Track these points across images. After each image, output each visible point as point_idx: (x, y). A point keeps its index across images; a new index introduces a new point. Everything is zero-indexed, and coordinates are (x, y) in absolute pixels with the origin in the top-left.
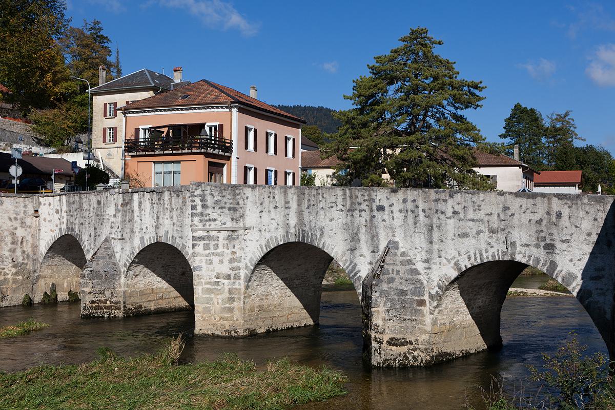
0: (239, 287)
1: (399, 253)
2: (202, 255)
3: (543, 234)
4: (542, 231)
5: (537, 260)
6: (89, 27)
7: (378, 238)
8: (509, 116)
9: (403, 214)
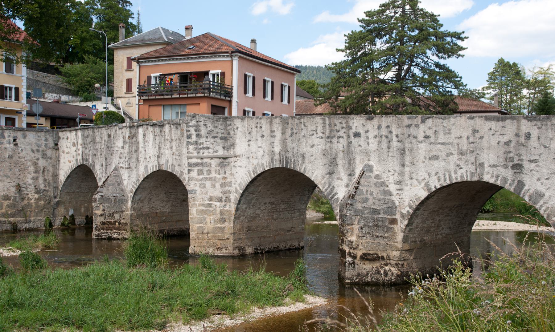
1: (373, 175)
2: (197, 180)
3: (511, 155)
4: (510, 152)
5: (505, 180)
7: (354, 162)
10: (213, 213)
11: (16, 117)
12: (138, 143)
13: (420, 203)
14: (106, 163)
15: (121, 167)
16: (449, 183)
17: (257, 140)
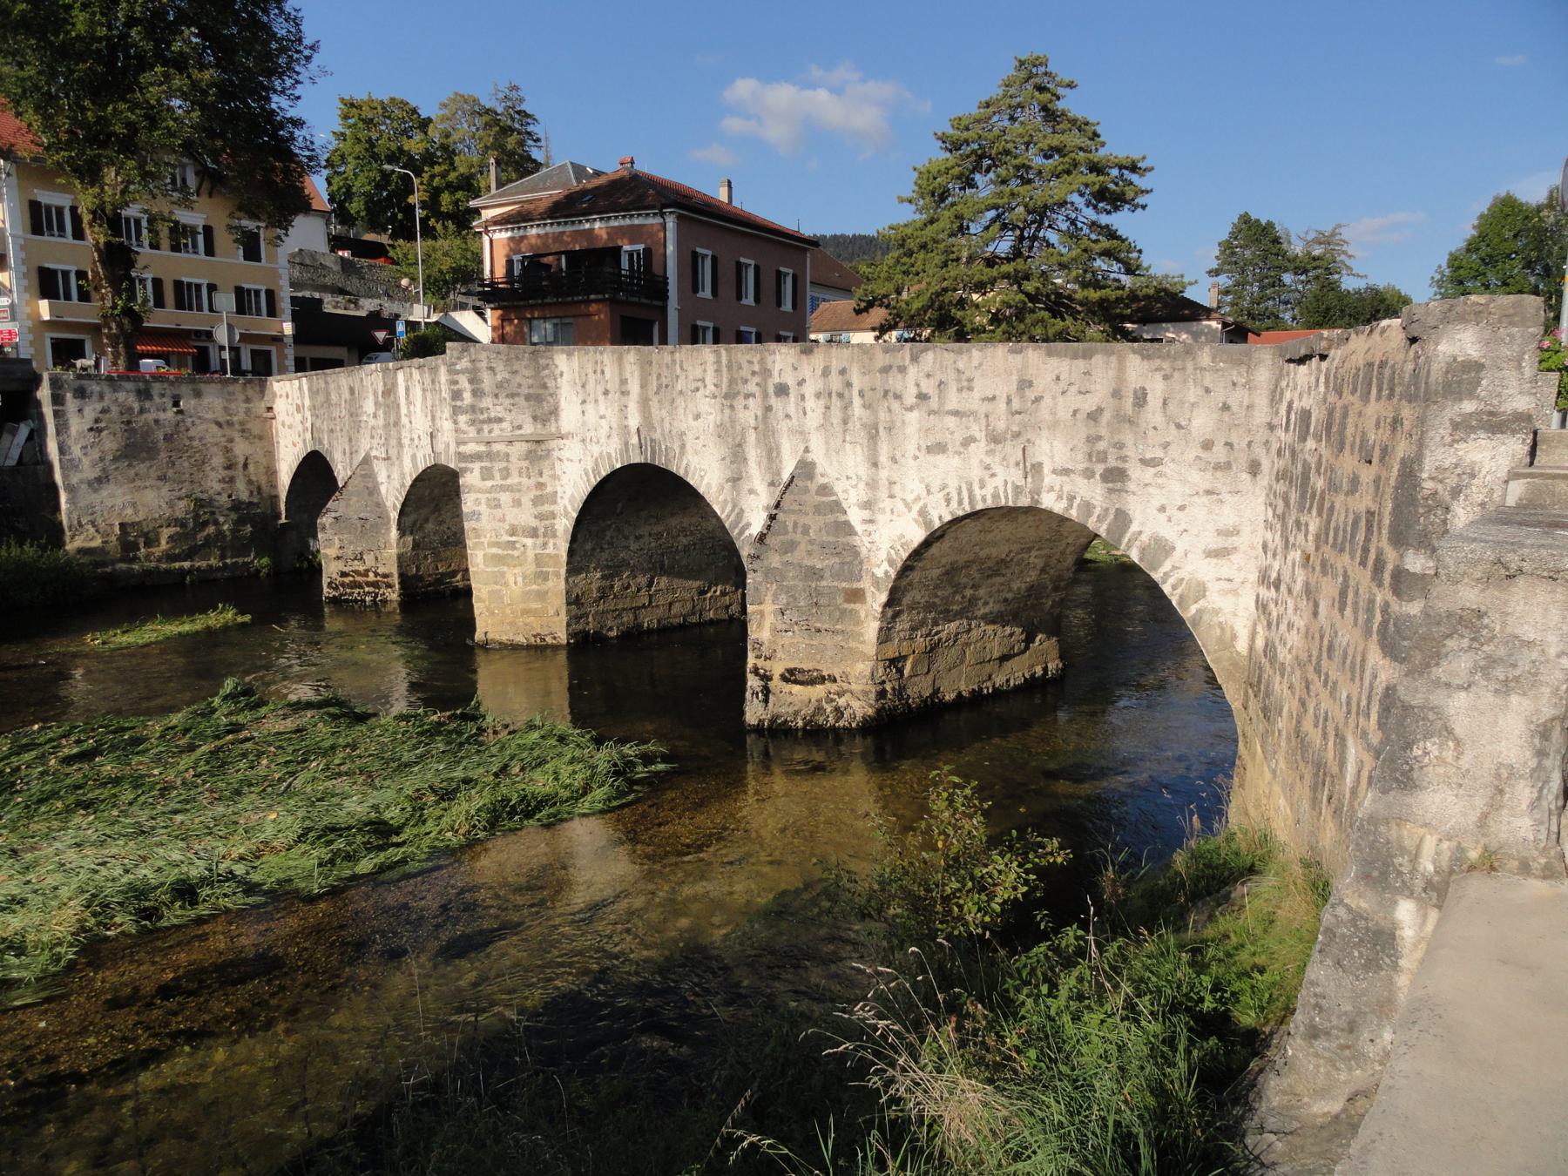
0: (556, 552)
1: (813, 487)
2: (480, 491)
3: (1101, 445)
4: (1100, 438)
5: (1087, 507)
6: (501, 95)
7: (778, 453)
8: (1225, 236)
9: (822, 402)
10: (519, 561)
11: (273, 349)
12: (398, 406)
13: (910, 556)
14: (351, 447)
15: (376, 457)
16: (968, 509)
17: (596, 401)
